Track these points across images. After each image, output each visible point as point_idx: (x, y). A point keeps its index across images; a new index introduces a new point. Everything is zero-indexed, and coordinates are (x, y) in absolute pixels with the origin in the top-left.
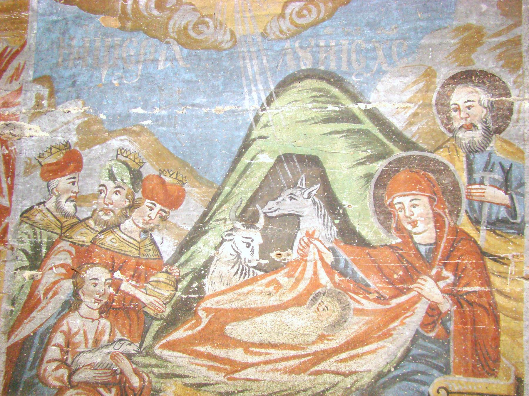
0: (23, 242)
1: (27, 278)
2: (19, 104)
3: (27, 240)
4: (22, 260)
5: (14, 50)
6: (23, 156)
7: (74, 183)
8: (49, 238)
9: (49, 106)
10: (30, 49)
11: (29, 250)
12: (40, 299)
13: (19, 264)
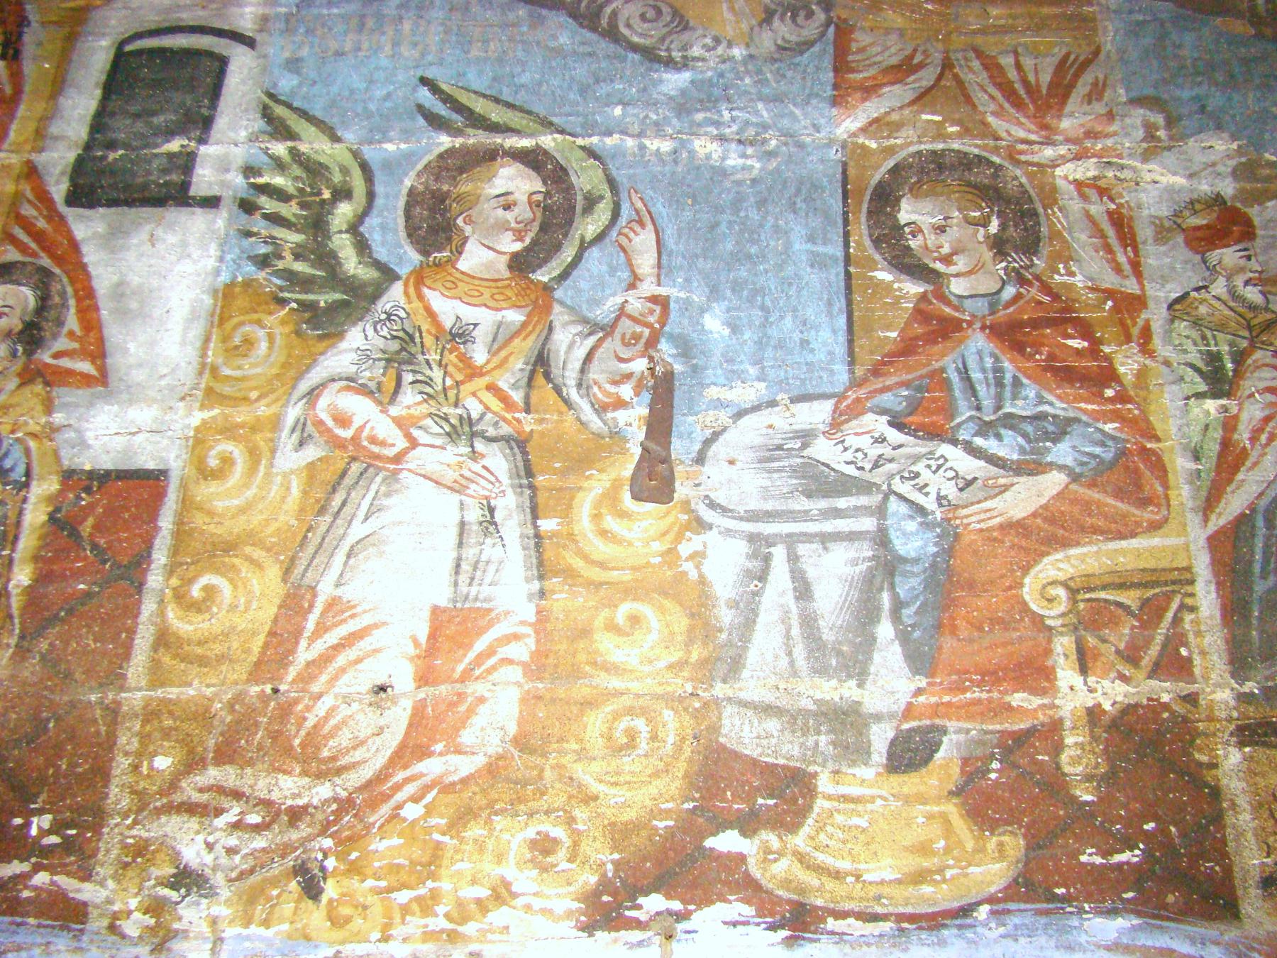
0: (1185, 352)
1: (1212, 411)
2: (1115, 134)
3: (1191, 348)
4: (1192, 382)
5: (1082, 58)
6: (1146, 212)
7: (1249, 258)
8: (1231, 345)
9: (1171, 138)
10: (1108, 56)
11: (1200, 364)
12: (1244, 448)
13: (1187, 389)
